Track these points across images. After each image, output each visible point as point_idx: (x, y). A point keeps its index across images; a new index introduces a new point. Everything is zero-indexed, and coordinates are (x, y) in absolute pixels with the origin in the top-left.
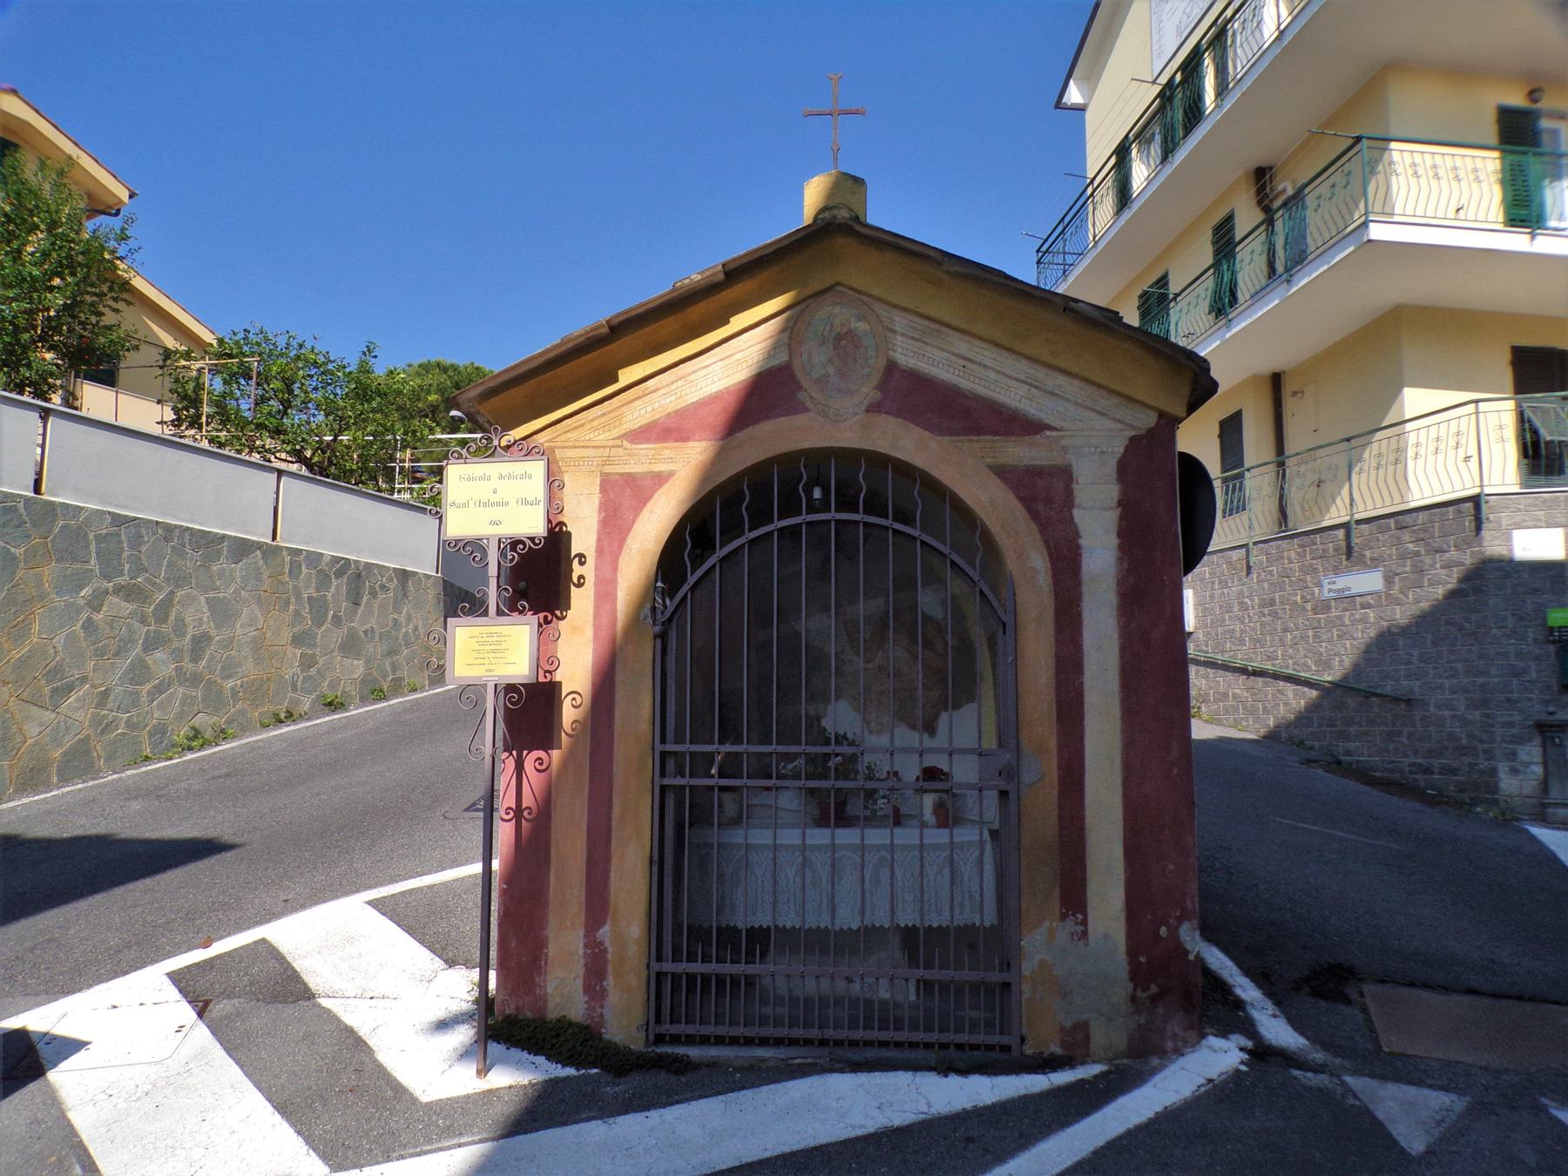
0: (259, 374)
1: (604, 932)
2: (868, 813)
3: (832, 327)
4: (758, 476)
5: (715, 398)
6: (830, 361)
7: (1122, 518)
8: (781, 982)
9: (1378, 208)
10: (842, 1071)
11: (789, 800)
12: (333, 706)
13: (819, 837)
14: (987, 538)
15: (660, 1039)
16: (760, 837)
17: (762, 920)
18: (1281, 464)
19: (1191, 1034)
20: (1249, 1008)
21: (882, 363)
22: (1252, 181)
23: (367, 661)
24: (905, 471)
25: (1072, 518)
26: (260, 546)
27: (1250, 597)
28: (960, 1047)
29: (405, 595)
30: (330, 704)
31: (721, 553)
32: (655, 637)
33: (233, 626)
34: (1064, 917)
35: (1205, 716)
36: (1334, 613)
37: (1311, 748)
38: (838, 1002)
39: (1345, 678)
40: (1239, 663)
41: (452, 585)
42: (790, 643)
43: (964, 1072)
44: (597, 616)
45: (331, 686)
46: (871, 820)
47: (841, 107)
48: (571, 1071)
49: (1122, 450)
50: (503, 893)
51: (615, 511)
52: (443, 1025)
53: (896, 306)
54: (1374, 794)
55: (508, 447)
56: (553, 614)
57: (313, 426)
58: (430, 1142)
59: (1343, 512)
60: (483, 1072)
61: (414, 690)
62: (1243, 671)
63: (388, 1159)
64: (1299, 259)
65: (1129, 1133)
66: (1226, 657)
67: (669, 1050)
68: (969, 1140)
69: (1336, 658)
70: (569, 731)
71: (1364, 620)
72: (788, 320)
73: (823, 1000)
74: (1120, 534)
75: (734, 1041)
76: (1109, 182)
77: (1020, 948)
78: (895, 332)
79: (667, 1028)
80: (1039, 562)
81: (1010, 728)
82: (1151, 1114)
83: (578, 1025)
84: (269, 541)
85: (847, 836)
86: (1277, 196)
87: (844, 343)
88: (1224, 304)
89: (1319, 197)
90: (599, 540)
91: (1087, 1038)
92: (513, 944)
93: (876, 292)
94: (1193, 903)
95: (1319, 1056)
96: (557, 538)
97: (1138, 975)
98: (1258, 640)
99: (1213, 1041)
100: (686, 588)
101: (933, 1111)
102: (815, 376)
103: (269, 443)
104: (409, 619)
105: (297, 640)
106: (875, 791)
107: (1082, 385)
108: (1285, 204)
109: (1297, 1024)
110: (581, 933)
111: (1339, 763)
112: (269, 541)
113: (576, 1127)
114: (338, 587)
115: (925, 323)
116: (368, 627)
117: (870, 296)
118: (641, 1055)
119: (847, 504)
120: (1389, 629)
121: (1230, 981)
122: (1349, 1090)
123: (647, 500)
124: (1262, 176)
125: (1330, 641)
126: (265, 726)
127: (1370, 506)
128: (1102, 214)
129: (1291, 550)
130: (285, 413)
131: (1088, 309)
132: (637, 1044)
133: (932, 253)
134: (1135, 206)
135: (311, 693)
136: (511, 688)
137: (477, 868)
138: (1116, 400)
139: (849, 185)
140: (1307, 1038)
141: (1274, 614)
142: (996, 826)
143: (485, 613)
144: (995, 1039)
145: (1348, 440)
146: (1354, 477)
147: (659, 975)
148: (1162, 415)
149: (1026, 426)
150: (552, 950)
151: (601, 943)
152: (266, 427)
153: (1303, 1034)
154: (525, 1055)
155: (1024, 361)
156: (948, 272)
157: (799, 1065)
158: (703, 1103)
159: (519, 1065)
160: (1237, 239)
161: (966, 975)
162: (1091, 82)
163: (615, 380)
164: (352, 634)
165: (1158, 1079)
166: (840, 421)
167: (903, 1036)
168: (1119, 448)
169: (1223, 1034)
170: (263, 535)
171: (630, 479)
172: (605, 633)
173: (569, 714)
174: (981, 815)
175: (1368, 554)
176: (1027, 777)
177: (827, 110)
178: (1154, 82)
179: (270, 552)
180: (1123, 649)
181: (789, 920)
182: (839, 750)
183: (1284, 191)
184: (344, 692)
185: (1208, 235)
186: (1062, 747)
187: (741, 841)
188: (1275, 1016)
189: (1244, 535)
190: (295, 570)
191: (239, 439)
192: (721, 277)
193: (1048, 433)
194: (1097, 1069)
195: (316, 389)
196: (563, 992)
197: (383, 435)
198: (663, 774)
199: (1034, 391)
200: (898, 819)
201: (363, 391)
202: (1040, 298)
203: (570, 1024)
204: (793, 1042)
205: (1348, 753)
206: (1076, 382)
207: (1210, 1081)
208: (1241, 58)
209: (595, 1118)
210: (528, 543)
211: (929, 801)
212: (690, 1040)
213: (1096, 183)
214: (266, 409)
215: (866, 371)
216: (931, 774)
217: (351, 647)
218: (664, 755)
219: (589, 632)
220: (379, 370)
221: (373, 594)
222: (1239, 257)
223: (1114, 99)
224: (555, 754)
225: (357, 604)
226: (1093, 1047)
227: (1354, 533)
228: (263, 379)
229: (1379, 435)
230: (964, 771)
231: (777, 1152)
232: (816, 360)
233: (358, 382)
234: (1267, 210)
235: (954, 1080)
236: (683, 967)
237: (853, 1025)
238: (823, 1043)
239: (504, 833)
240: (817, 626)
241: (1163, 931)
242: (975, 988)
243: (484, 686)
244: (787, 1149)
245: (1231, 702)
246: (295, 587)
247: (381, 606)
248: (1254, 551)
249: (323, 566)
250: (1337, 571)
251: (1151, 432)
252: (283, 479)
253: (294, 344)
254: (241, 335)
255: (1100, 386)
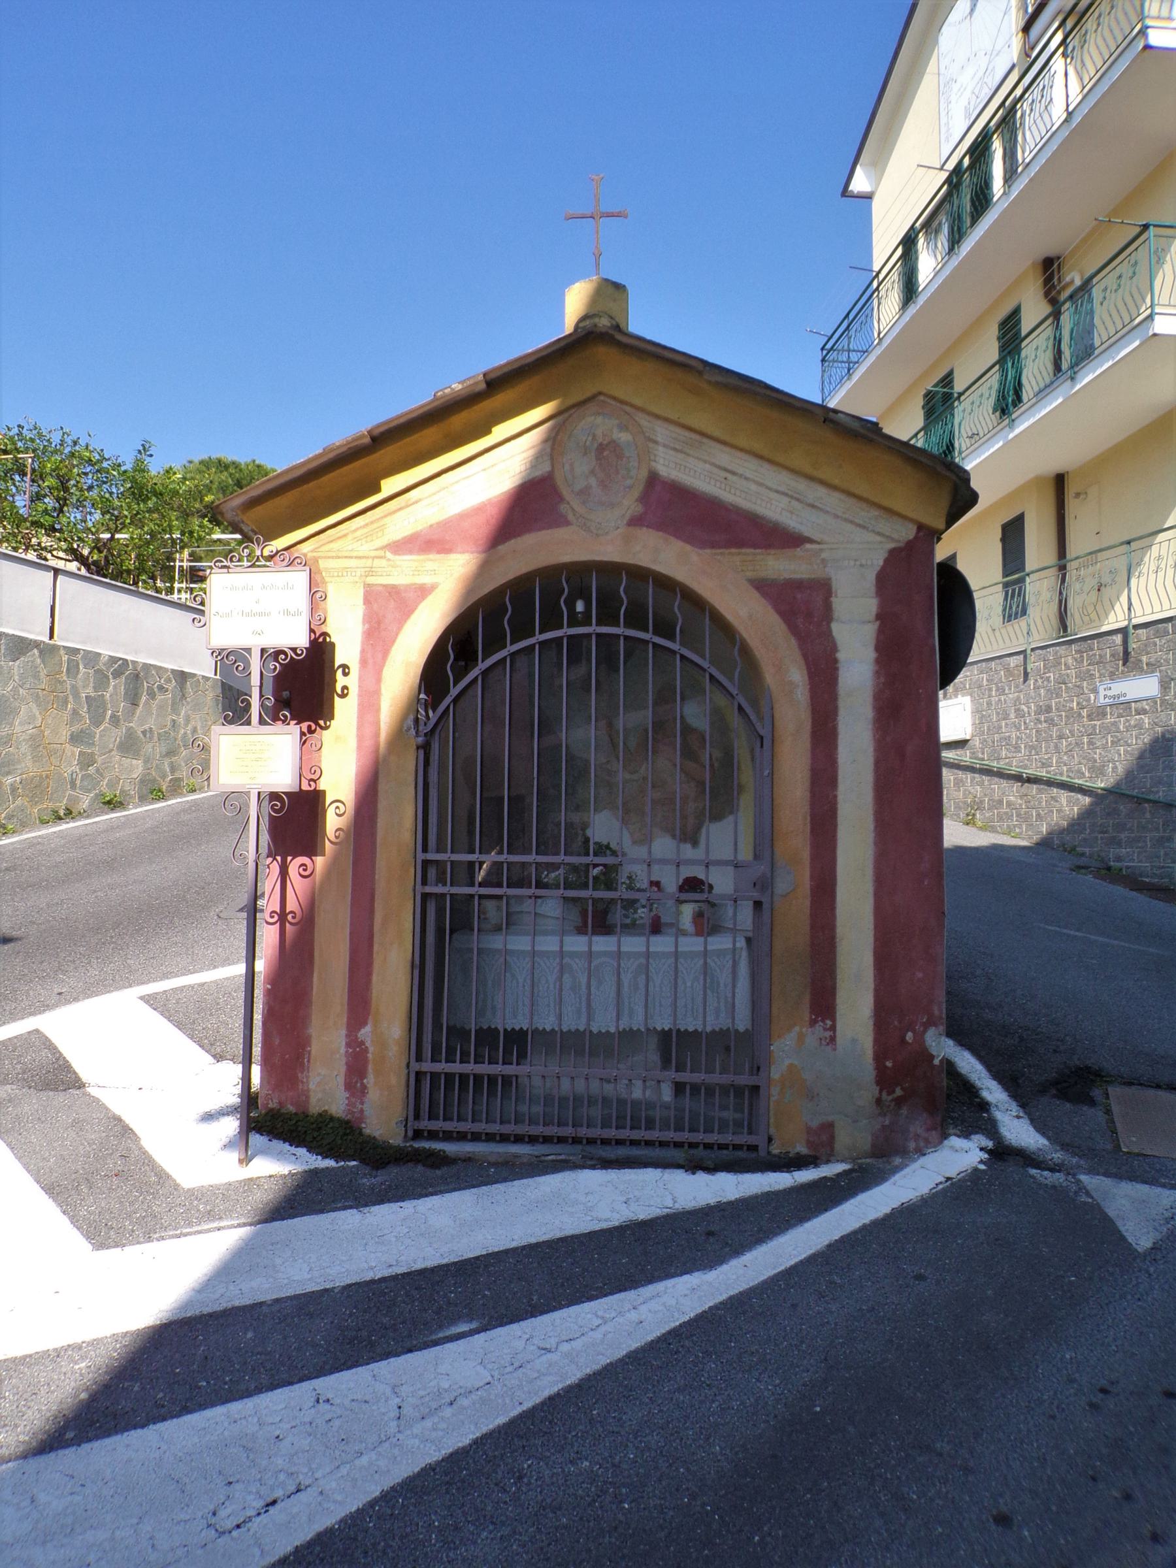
0: (33, 470)
1: (365, 1033)
2: (628, 921)
3: (594, 436)
4: (520, 588)
5: (479, 509)
6: (592, 472)
7: (880, 631)
8: (537, 1081)
9: (1164, 299)
10: (593, 1167)
11: (551, 906)
12: (112, 804)
13: (577, 943)
14: (745, 651)
15: (418, 1135)
16: (520, 943)
17: (520, 1022)
18: (1062, 568)
19: (934, 1135)
20: (993, 1109)
21: (644, 474)
22: (1040, 270)
23: (146, 761)
24: (665, 584)
25: (830, 631)
26: (37, 644)
27: (1027, 704)
28: (708, 1146)
29: (184, 696)
30: (109, 802)
31: (482, 666)
32: (418, 748)
33: (11, 724)
34: (813, 1023)
35: (979, 824)
36: (1109, 719)
37: (1083, 854)
38: (592, 1101)
39: (1118, 784)
40: (1014, 770)
41: (231, 688)
42: (549, 757)
43: (712, 1170)
44: (360, 727)
45: (111, 785)
46: (631, 928)
47: (604, 208)
48: (330, 1163)
49: (881, 563)
50: (269, 994)
51: (379, 623)
52: (208, 1117)
53: (658, 417)
54: (1140, 900)
55: (270, 558)
56: (317, 724)
57: (90, 524)
58: (190, 1225)
59: (1121, 617)
60: (246, 1160)
61: (193, 791)
62: (1018, 778)
63: (150, 1240)
64: (1086, 354)
65: (864, 1228)
66: (1002, 764)
67: (426, 1145)
68: (710, 1234)
69: (1111, 764)
70: (333, 838)
71: (1139, 726)
72: (551, 430)
73: (577, 1099)
74: (877, 648)
75: (490, 1138)
76: (895, 276)
77: (770, 1052)
78: (656, 442)
79: (425, 1124)
80: (797, 675)
81: (766, 839)
82: (887, 1210)
83: (339, 1119)
84: (46, 639)
85: (603, 944)
86: (1064, 288)
87: (606, 454)
88: (1009, 402)
89: (1105, 290)
90: (363, 651)
91: (832, 1138)
92: (277, 1042)
93: (638, 402)
94: (940, 1009)
95: (1058, 1156)
96: (320, 651)
97: (884, 1079)
98: (1032, 747)
99: (955, 1141)
100: (448, 700)
101: (677, 1206)
102: (578, 487)
103: (46, 541)
104: (188, 720)
105: (75, 739)
106: (635, 901)
107: (843, 497)
108: (1071, 297)
109: (1040, 1126)
110: (344, 1032)
111: (1109, 869)
112: (46, 639)
113: (333, 1215)
114: (116, 688)
115: (687, 434)
116: (146, 727)
117: (632, 406)
118: (399, 1149)
119: (608, 616)
120: (1163, 735)
121: (978, 1084)
122: (1082, 1189)
123: (412, 611)
124: (1050, 267)
125: (1104, 747)
126: (44, 822)
127: (1148, 610)
128: (888, 309)
129: (1069, 656)
130: (61, 511)
131: (848, 419)
132: (397, 1140)
133: (693, 363)
134: (921, 300)
135: (89, 791)
136: (274, 796)
137: (241, 969)
138: (875, 512)
139: (611, 291)
140: (1048, 1139)
141: (1050, 721)
142: (750, 934)
143: (248, 723)
144: (743, 1139)
145: (1129, 543)
146: (1134, 581)
147: (419, 1075)
148: (921, 527)
149: (784, 539)
150: (315, 1048)
151: (362, 1043)
152: (41, 526)
153: (1043, 1134)
154: (286, 1146)
155: (784, 473)
156: (709, 382)
157: (553, 1161)
158: (456, 1195)
159: (280, 1156)
160: (1023, 333)
161: (716, 1078)
162: (879, 166)
163: (377, 489)
164: (130, 734)
165: (897, 1177)
166: (602, 534)
167: (654, 1135)
168: (878, 560)
169: (966, 1135)
170: (39, 634)
171: (393, 591)
172: (368, 743)
173: (333, 822)
174: (735, 924)
175: (1144, 659)
176: (782, 886)
177: (588, 212)
178: (942, 169)
179: (48, 651)
180: (877, 763)
181: (547, 1022)
182: (597, 860)
183: (1072, 282)
184: (122, 791)
185: (993, 331)
186: (814, 858)
187: (500, 946)
188: (1018, 1117)
189: (1022, 640)
190: (73, 669)
191: (15, 535)
192: (483, 386)
193: (808, 546)
194: (839, 1168)
195: (90, 488)
196: (325, 1088)
197: (152, 536)
198: (424, 882)
199: (795, 503)
200: (656, 928)
201: (139, 490)
202: (798, 409)
203: (332, 1119)
204: (547, 1140)
205: (1119, 859)
206: (837, 495)
207: (948, 1179)
208: (1030, 139)
209: (351, 1207)
210: (290, 653)
211: (688, 910)
212: (448, 1136)
213: (881, 277)
214: (40, 507)
215: (629, 482)
216: (692, 885)
217: (129, 746)
218: (426, 863)
219: (353, 743)
220: (155, 468)
221: (152, 695)
222: (1023, 354)
223: (901, 186)
224: (319, 860)
225: (135, 704)
226: (838, 1146)
227: (1131, 639)
228: (38, 476)
229: (1162, 537)
230: (722, 882)
231: (524, 1242)
232: (578, 470)
233: (134, 480)
234: (1053, 301)
235: (701, 1177)
236: (442, 1067)
237: (605, 1124)
238: (576, 1141)
239: (268, 936)
240: (582, 737)
241: (909, 1036)
242: (725, 1090)
243: (248, 793)
244: (533, 1240)
245: (1005, 809)
246: (73, 687)
247: (160, 707)
248: (1032, 657)
249: (101, 666)
250: (1113, 676)
251: (910, 545)
252: (60, 577)
253: (69, 440)
254: (16, 430)
255: (860, 498)
